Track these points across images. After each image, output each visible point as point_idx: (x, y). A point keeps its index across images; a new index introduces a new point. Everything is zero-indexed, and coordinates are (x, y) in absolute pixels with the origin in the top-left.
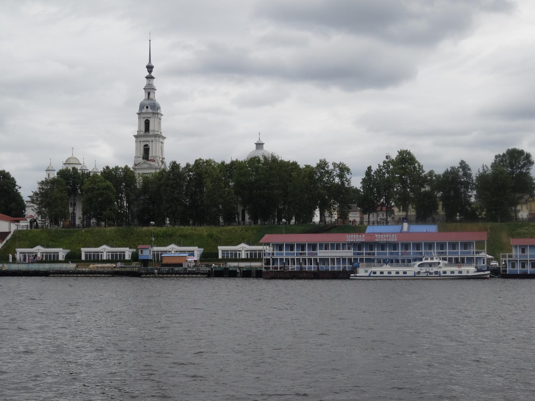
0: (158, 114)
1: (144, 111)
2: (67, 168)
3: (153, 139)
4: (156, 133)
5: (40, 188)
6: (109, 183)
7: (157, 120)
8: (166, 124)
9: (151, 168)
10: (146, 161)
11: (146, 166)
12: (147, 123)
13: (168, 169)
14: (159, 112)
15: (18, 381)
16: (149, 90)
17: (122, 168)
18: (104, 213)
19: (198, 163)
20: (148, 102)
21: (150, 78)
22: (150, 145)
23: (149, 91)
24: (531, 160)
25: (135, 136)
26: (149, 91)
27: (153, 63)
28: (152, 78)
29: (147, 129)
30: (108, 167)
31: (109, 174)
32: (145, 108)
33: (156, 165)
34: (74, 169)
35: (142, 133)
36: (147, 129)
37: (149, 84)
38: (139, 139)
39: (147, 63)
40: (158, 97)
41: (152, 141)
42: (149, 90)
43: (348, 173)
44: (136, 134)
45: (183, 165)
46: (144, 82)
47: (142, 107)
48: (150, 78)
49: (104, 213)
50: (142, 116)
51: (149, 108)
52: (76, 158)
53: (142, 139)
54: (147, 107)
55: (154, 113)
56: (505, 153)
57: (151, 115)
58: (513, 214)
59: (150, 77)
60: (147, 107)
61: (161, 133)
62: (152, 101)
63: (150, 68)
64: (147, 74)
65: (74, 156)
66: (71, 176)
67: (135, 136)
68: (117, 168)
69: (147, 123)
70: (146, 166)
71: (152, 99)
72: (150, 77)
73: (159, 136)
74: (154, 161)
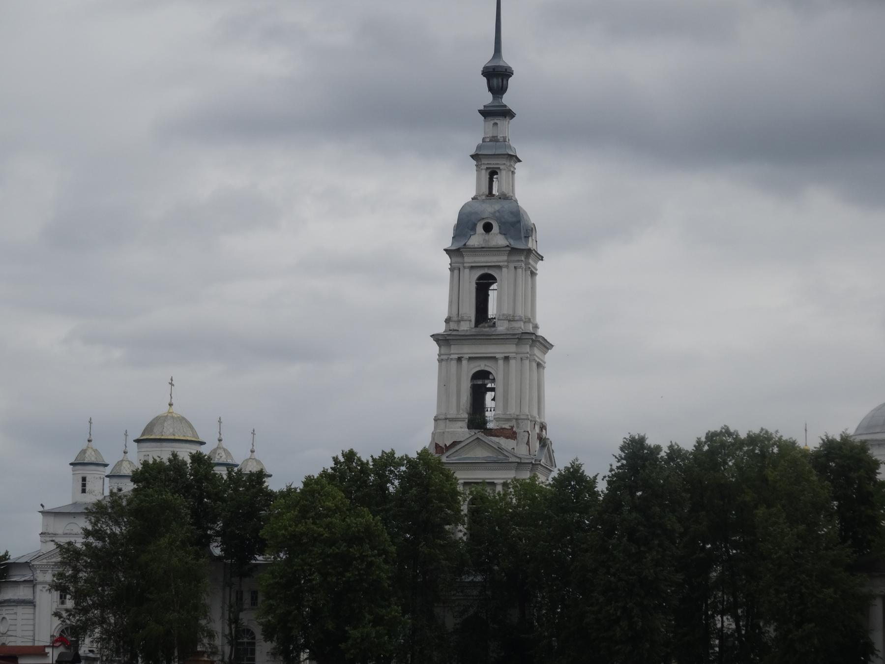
0: (529, 251)
1: (476, 240)
2: (175, 455)
3: (510, 349)
4: (520, 327)
5: (87, 533)
6: (367, 517)
8: (557, 295)
9: (501, 461)
10: (481, 435)
11: (480, 453)
13: (140, 467)
14: (530, 245)
17: (409, 461)
18: (355, 633)
20: (489, 209)
22: (497, 370)
23: (493, 163)
24: (281, 492)
25: (437, 338)
26: (493, 163)
27: (508, 59)
28: (507, 114)
30: (350, 456)
31: (353, 480)
32: (480, 229)
33: (522, 451)
34: (197, 459)
35: (466, 327)
37: (494, 139)
38: (456, 350)
39: (486, 57)
41: (507, 359)
43: (85, 530)
44: (441, 328)
49: (355, 633)
50: (469, 260)
51: (496, 228)
52: (182, 420)
53: (468, 350)
54: (488, 228)
55: (513, 251)
57: (501, 259)
59: (497, 113)
60: (488, 228)
61: (536, 327)
62: (506, 205)
64: (488, 98)
65: (177, 410)
66: (587, 482)
67: (437, 338)
68: (387, 461)
70: (480, 453)
71: (504, 197)
72: (497, 113)
73: (531, 340)
74: (511, 435)
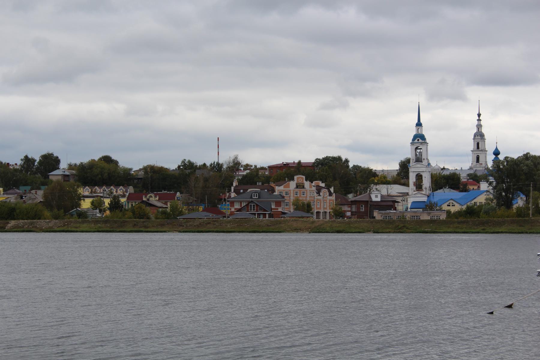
7: (425, 146)
12: (478, 144)
15: (353, 356)
16: (479, 126)
19: (299, 163)
21: (479, 120)
29: (478, 148)
36: (478, 148)
39: (478, 112)
40: (484, 130)
42: (479, 126)
45: (3, 163)
46: (476, 123)
47: (475, 136)
48: (479, 120)
56: (208, 164)
58: (25, 166)
63: (479, 115)
64: (478, 118)
69: (478, 144)
